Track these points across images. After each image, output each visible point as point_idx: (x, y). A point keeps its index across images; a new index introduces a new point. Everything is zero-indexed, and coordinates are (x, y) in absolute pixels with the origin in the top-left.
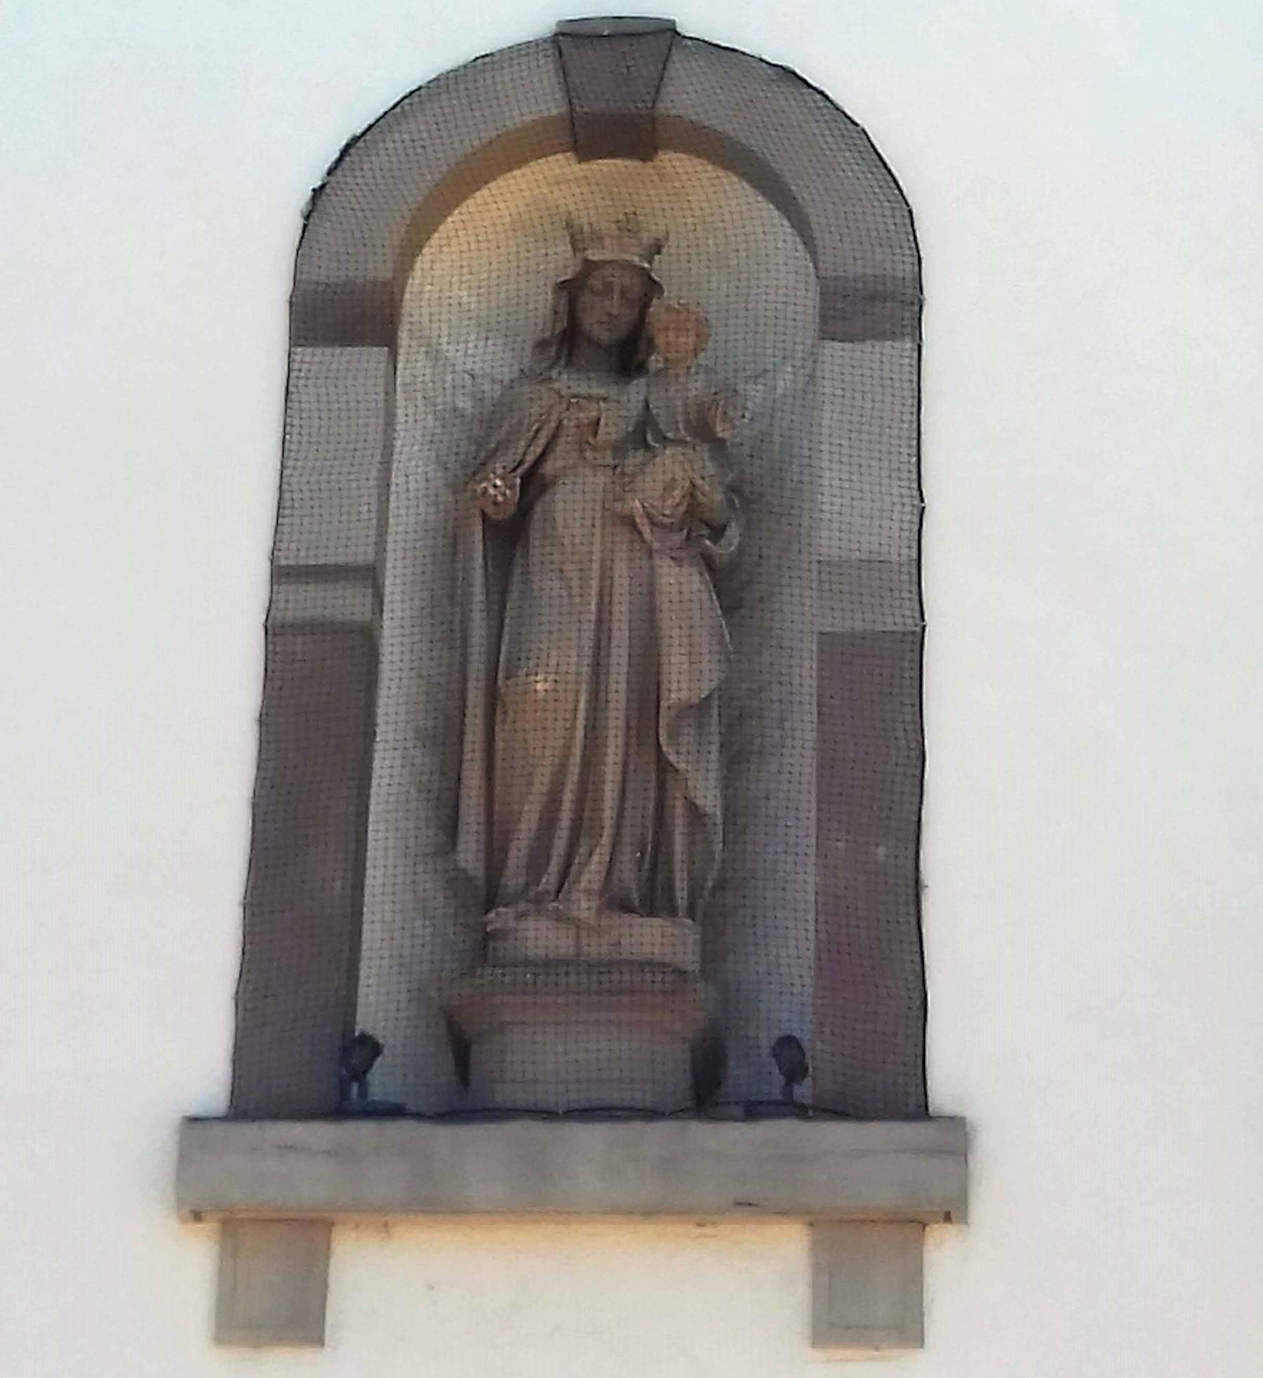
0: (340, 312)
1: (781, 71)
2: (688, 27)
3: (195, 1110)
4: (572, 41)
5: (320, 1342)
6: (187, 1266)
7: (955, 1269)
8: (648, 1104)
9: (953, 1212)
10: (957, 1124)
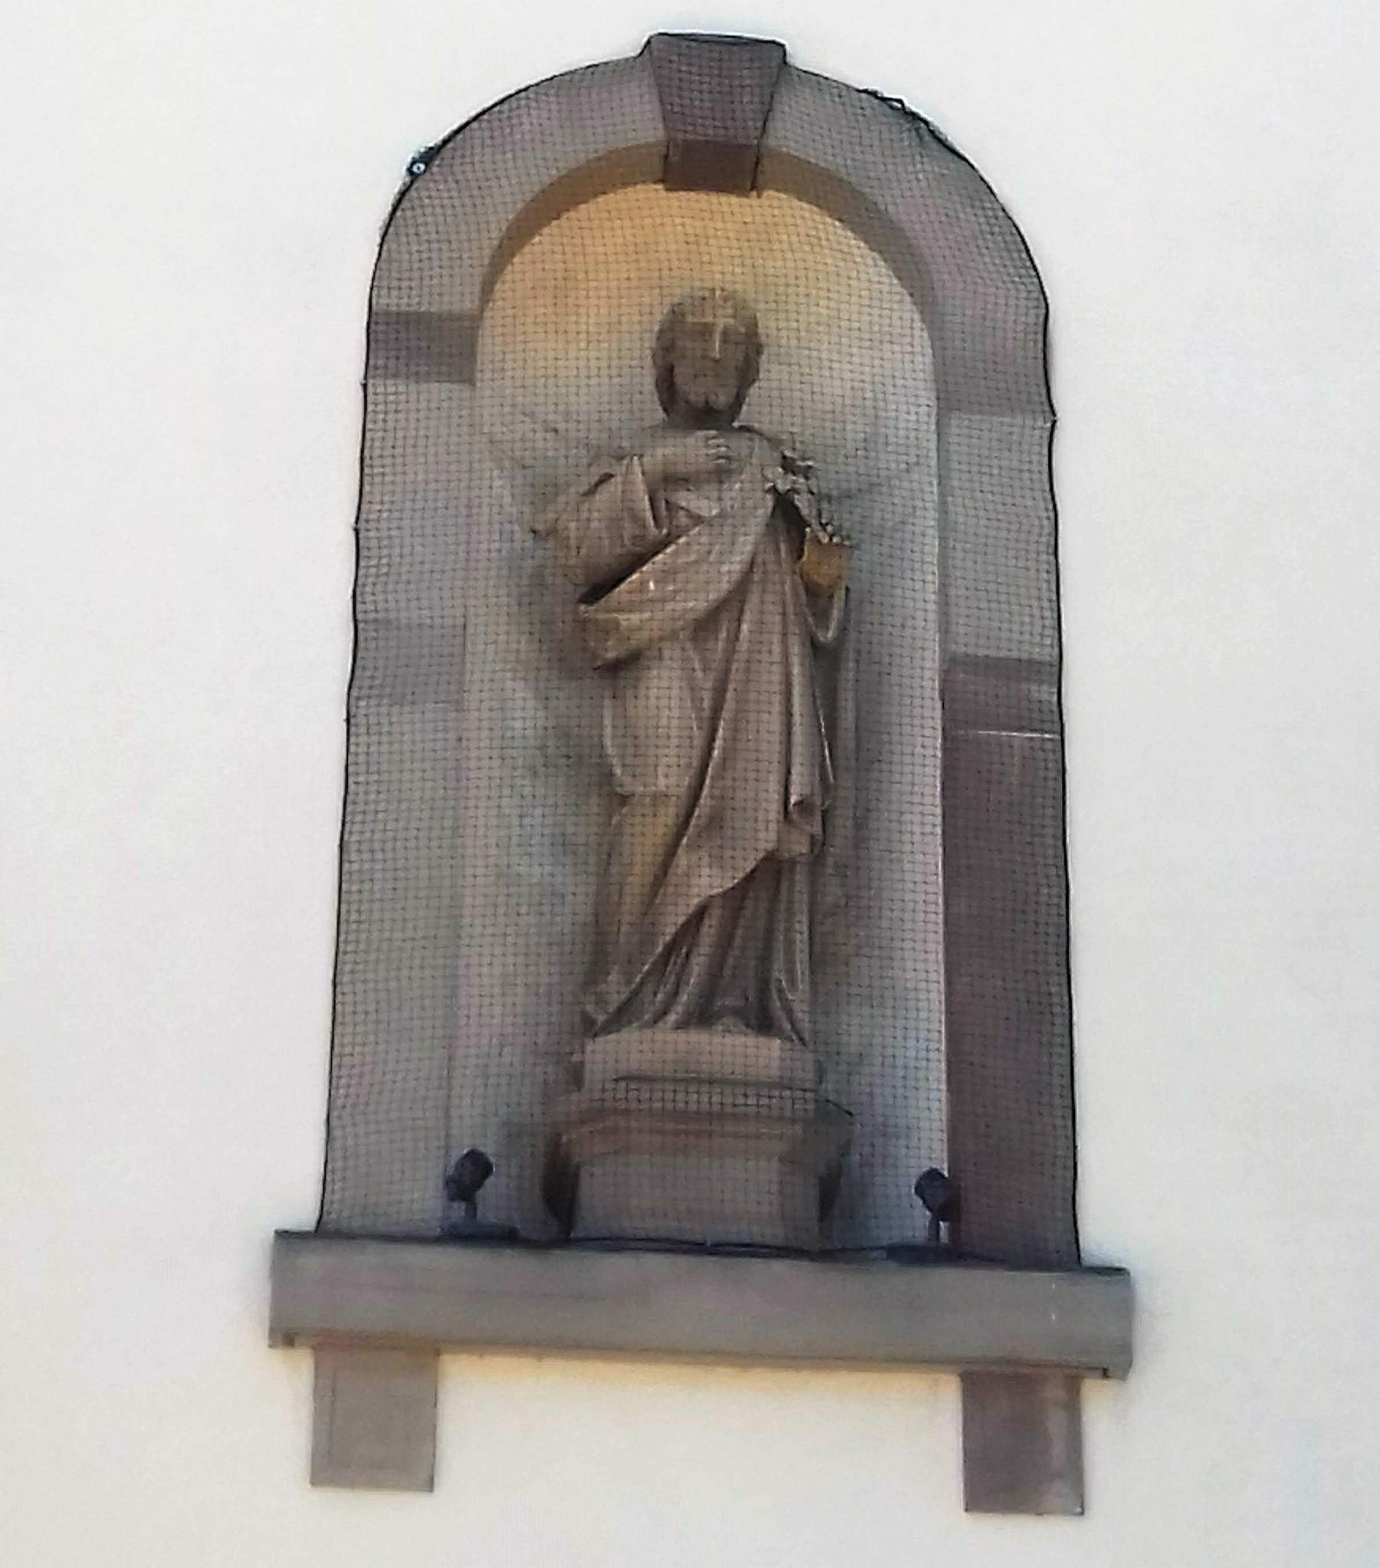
0: (412, 342)
1: (1034, 318)
2: (801, 57)
3: (288, 1227)
4: (673, 57)
5: (429, 1485)
6: (280, 1397)
7: (1116, 1431)
8: (780, 1242)
9: (1114, 1362)
10: (1116, 1273)
